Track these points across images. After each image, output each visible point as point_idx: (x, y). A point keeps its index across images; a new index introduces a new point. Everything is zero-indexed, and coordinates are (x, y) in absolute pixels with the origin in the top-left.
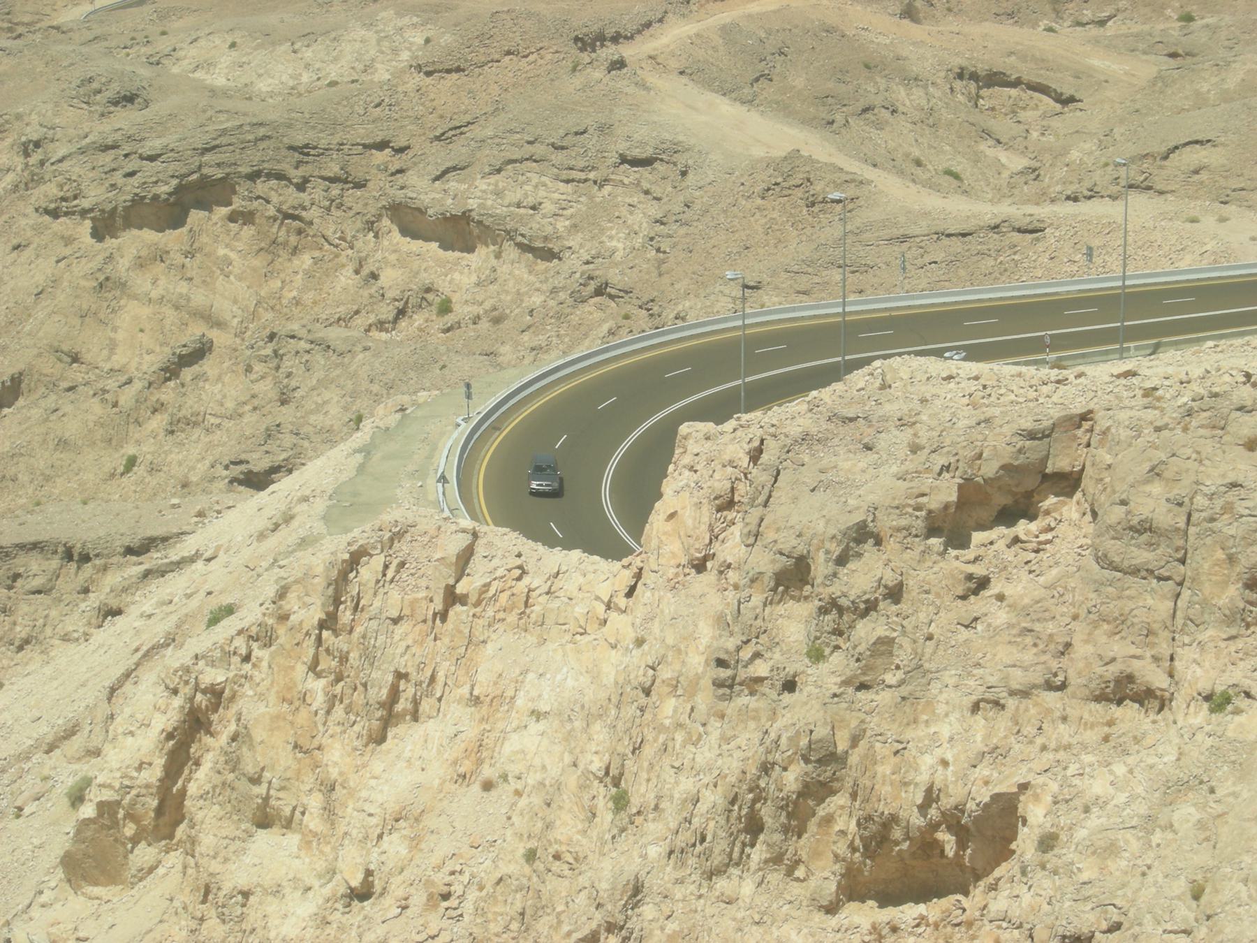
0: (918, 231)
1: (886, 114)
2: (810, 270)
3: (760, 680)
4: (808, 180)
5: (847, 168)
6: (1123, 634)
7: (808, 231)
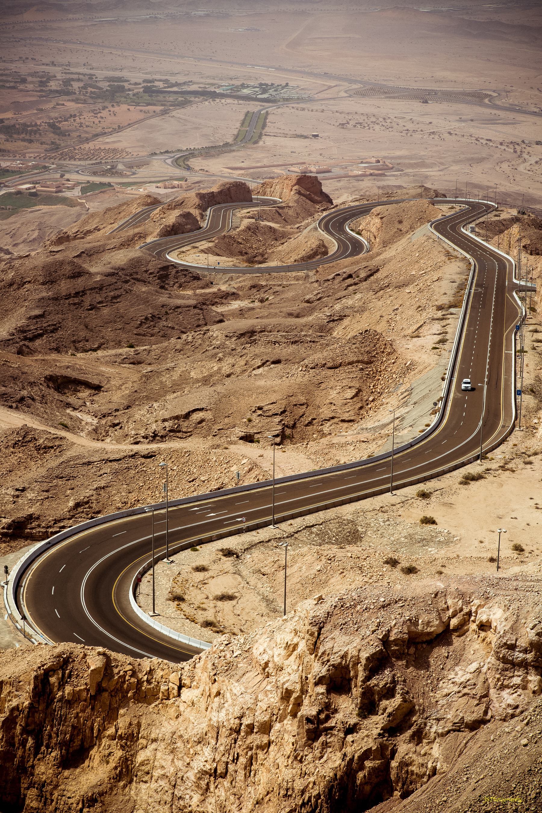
0: (95, 459)
1: (30, 401)
2: (47, 480)
3: (332, 728)
4: (35, 438)
5: (52, 432)
6: (518, 693)
7: (39, 462)
